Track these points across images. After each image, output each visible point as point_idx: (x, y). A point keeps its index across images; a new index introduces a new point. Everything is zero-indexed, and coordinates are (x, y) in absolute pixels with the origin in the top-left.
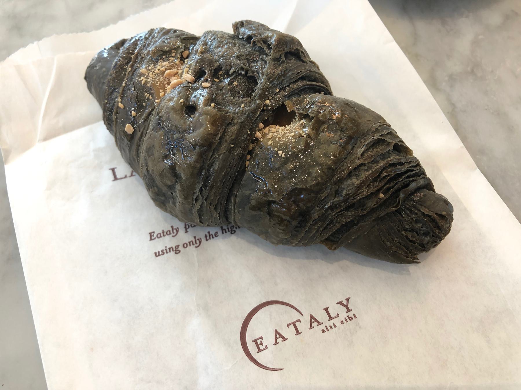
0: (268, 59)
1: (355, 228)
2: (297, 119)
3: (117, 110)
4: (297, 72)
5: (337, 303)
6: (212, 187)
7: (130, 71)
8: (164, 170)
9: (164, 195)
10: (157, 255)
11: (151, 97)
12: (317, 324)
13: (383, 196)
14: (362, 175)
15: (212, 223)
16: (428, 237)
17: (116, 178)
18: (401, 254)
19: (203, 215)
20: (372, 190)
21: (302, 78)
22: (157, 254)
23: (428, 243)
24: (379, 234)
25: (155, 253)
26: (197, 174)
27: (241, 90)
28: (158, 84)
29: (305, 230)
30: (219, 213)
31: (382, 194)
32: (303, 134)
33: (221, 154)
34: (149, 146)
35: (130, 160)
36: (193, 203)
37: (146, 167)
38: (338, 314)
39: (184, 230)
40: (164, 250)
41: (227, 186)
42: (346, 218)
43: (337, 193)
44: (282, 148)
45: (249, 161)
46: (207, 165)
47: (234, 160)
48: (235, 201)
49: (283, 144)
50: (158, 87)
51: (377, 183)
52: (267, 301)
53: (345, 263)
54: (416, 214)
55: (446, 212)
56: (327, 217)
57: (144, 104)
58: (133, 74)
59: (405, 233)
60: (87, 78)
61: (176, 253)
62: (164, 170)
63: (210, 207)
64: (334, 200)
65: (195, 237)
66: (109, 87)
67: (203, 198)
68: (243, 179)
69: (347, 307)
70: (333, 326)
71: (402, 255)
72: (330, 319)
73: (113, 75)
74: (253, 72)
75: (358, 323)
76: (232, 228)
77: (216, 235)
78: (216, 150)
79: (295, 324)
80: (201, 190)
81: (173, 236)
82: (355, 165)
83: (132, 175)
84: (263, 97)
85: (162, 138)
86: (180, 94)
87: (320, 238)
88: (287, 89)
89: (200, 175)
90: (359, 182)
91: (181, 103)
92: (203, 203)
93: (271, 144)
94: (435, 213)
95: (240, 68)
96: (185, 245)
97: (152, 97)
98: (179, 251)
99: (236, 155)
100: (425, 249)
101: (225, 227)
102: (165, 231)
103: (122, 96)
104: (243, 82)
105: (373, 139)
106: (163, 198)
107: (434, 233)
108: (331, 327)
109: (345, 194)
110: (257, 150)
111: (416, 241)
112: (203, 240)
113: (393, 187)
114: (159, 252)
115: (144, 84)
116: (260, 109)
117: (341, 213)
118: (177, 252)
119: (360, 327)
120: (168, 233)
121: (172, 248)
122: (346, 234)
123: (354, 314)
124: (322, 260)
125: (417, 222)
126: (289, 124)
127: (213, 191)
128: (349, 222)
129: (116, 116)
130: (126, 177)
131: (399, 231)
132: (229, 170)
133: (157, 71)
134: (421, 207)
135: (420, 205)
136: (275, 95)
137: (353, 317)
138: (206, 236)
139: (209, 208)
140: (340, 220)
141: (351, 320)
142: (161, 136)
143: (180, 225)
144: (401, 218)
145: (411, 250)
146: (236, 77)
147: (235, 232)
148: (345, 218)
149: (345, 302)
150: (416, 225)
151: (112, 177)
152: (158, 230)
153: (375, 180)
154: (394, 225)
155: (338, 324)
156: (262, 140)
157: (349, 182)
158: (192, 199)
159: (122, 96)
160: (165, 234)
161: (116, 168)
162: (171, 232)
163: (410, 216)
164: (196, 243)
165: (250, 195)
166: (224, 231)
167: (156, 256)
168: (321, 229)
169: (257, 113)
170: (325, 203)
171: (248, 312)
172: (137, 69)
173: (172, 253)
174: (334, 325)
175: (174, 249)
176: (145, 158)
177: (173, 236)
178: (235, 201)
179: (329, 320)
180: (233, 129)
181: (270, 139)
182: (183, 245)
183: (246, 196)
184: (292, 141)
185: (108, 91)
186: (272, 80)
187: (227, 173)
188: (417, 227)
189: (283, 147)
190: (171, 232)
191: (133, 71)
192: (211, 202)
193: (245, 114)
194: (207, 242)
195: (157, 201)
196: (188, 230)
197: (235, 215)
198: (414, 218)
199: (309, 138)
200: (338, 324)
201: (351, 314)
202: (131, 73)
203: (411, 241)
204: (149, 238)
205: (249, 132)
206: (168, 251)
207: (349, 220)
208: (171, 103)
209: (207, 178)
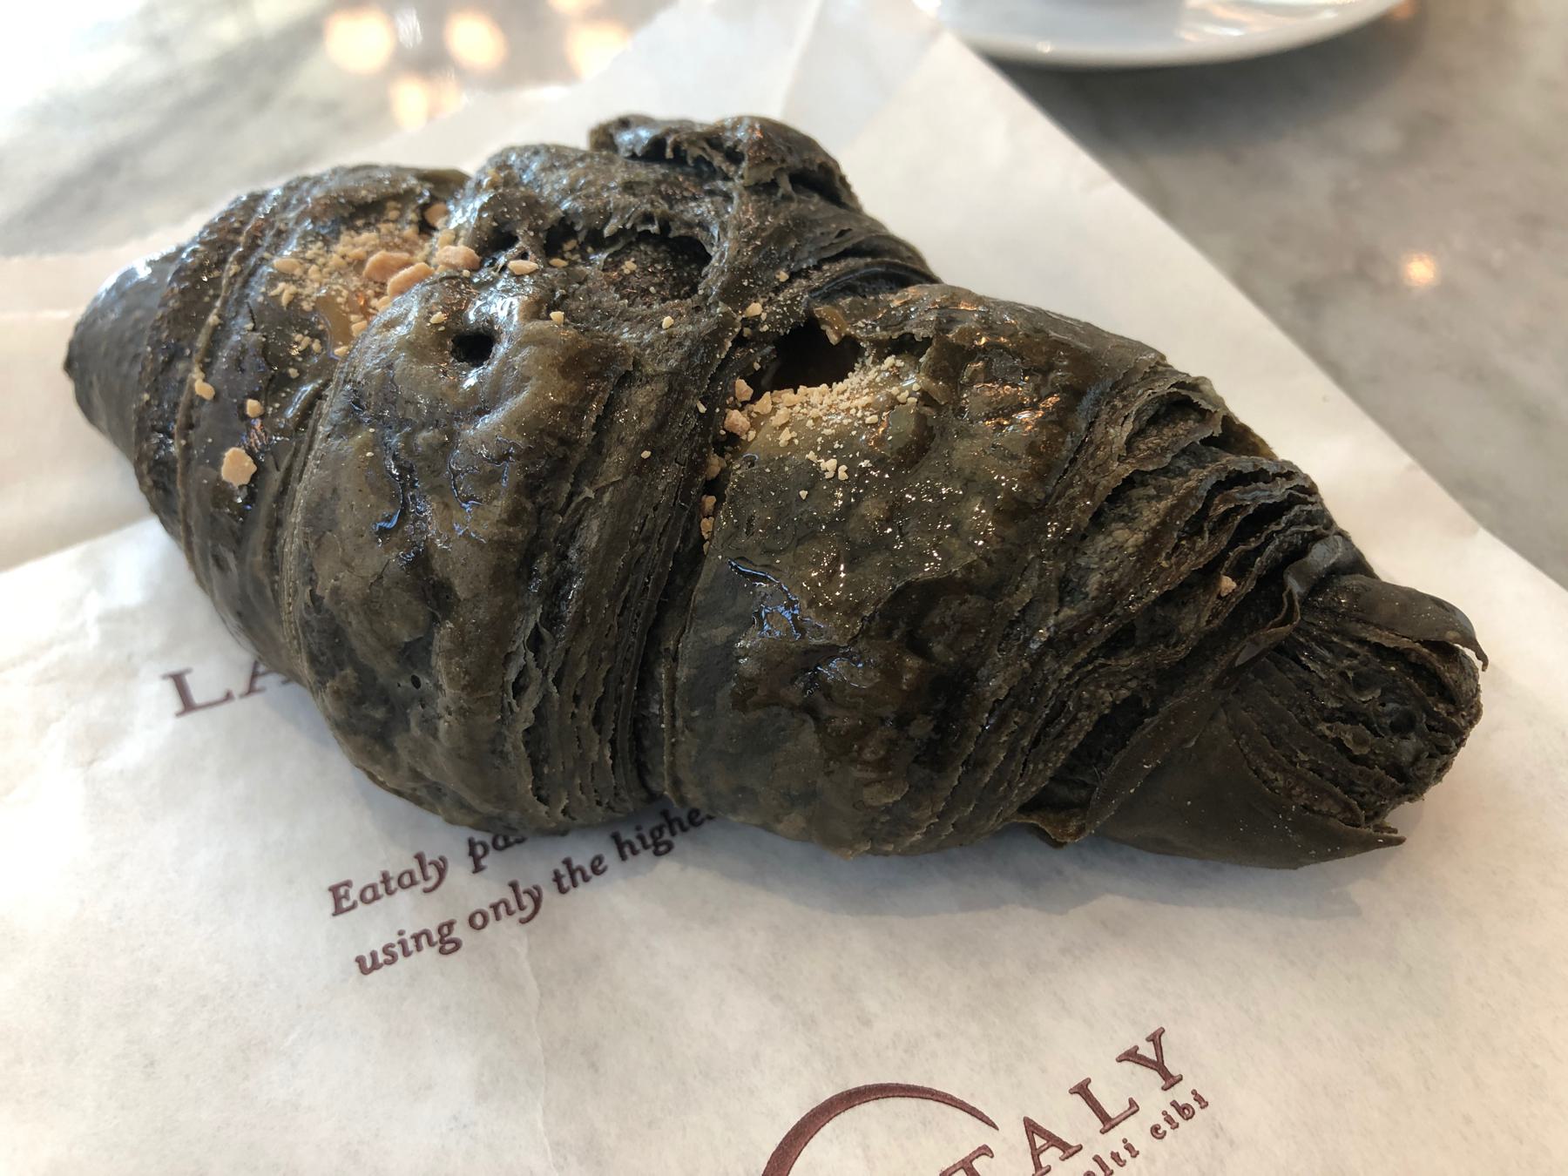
0: (735, 186)
1: (1149, 724)
2: (869, 362)
3: (189, 417)
4: (837, 228)
5: (1120, 1060)
6: (580, 623)
7: (235, 275)
8: (381, 577)
9: (385, 698)
10: (368, 965)
11: (316, 346)
12: (1061, 1153)
13: (1234, 585)
14: (1146, 513)
15: (583, 797)
16: (1412, 735)
17: (187, 705)
18: (1329, 815)
19: (545, 760)
20: (1191, 563)
21: (855, 252)
22: (369, 964)
23: (1417, 758)
24: (1237, 743)
25: (360, 960)
26: (518, 574)
27: (654, 285)
28: (342, 296)
29: (965, 757)
30: (613, 742)
31: (1230, 579)
32: (901, 398)
33: (608, 486)
34: (316, 498)
35: (244, 598)
36: (506, 702)
37: (310, 588)
38: (1132, 1103)
39: (470, 862)
40: (392, 945)
41: (638, 615)
42: (1114, 685)
43: (1066, 589)
44: (835, 451)
45: (712, 519)
46: (553, 531)
47: (655, 509)
48: (673, 679)
49: (837, 437)
50: (343, 307)
51: (1203, 539)
52: (842, 1093)
53: (1114, 903)
54: (1353, 655)
55: (1458, 631)
56: (1044, 689)
57: (293, 372)
58: (246, 284)
59: (1330, 729)
60: (75, 363)
61: (442, 951)
62: (381, 577)
63: (573, 714)
64: (1061, 616)
65: (514, 886)
66: (156, 344)
67: (545, 674)
68: (698, 586)
69: (1159, 1066)
70: (1125, 1155)
71: (1332, 819)
72: (1107, 1127)
73: (171, 303)
74: (689, 225)
75: (1220, 1124)
76: (657, 834)
77: (597, 867)
78: (584, 473)
79: (973, 1168)
80: (536, 642)
81: (426, 891)
82: (1107, 483)
83: (251, 690)
84: (735, 294)
85: (369, 454)
86: (427, 300)
87: (1021, 785)
88: (815, 275)
89: (530, 578)
90: (1139, 537)
91: (437, 325)
92: (546, 697)
93: (791, 441)
94: (1419, 642)
95: (638, 217)
96: (479, 920)
97: (322, 343)
98: (458, 945)
99: (664, 491)
100: (1409, 785)
101: (628, 835)
102: (394, 873)
103: (207, 360)
104: (655, 261)
105: (1152, 396)
106: (380, 714)
107: (1432, 715)
108: (1115, 1157)
109: (1095, 586)
110: (739, 472)
111: (1373, 757)
112: (549, 894)
113: (1258, 551)
114: (374, 955)
115: (290, 304)
116: (732, 331)
117: (1090, 667)
118: (449, 947)
119: (1232, 1143)
120: (406, 881)
121: (426, 933)
122: (1117, 761)
123: (1194, 1092)
124: (1025, 905)
125: (1360, 685)
126: (841, 377)
127: (586, 643)
128: (1125, 701)
129: (185, 437)
130: (228, 697)
131: (1306, 724)
132: (641, 547)
133: (334, 259)
134: (1363, 628)
135: (1358, 621)
136: (777, 290)
137: (1195, 1105)
138: (557, 878)
139: (569, 722)
140: (1093, 694)
141: (1187, 1119)
142: (363, 448)
143: (448, 840)
144: (1304, 675)
145: (1363, 795)
146: (629, 245)
147: (670, 846)
148: (1109, 686)
149: (1148, 1051)
150: (1362, 696)
151: (172, 701)
152: (364, 874)
153: (1194, 528)
154: (1286, 702)
155: (1142, 1141)
156: (752, 434)
157: (1102, 542)
158: (503, 688)
159: (207, 360)
160: (393, 884)
161: (188, 671)
162: (418, 876)
163: (1331, 666)
164: (521, 908)
165: (731, 642)
166: (627, 850)
167: (365, 971)
168: (1025, 743)
169: (722, 346)
170: (1025, 633)
171: (770, 1148)
172: (260, 265)
173: (429, 953)
174: (1127, 1148)
175: (436, 938)
176: (304, 550)
177: (426, 891)
178: (673, 679)
179: (1103, 1132)
180: (643, 397)
181: (783, 427)
182: (471, 920)
183: (717, 646)
184: (868, 420)
185: (155, 359)
186: (758, 243)
187: (634, 561)
188: (1364, 702)
189: (836, 446)
190: (418, 876)
191: (246, 272)
192: (578, 693)
193: (680, 345)
194: (567, 896)
195: (356, 733)
196: (484, 862)
197: (673, 745)
198: (1350, 668)
199: (925, 405)
200: (1142, 1141)
201: (1182, 1094)
202: (240, 280)
203: (1355, 760)
204: (330, 908)
205: (702, 409)
206: (411, 945)
207: (1124, 693)
208: (401, 330)
209: (558, 587)
